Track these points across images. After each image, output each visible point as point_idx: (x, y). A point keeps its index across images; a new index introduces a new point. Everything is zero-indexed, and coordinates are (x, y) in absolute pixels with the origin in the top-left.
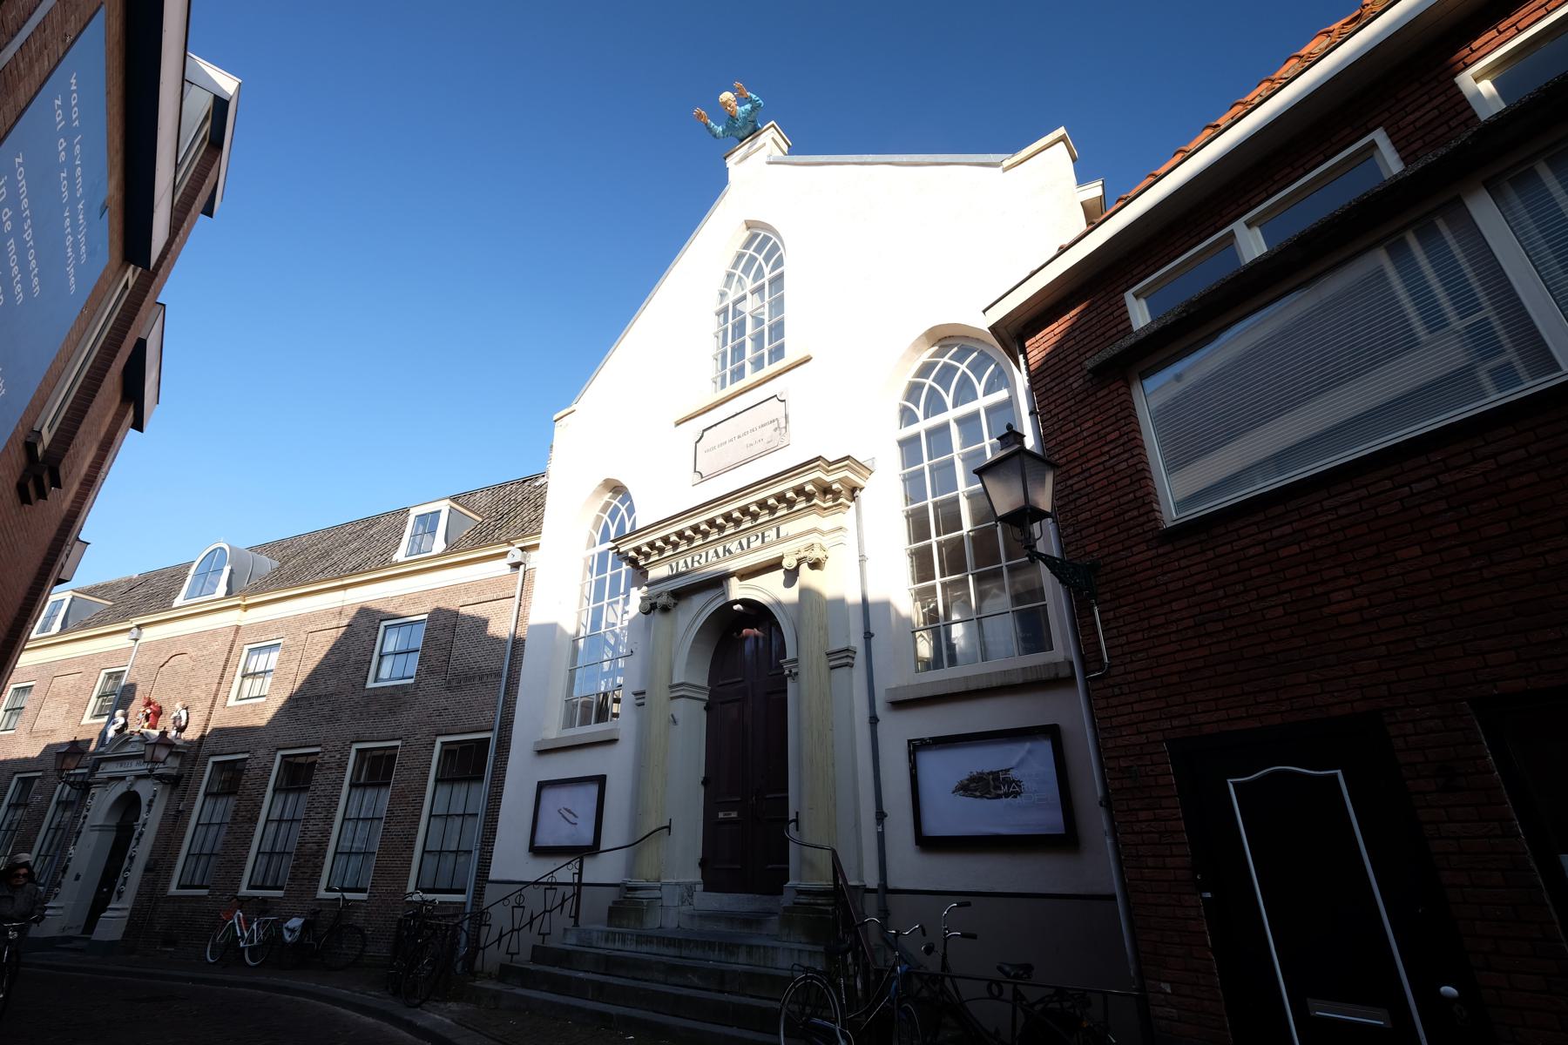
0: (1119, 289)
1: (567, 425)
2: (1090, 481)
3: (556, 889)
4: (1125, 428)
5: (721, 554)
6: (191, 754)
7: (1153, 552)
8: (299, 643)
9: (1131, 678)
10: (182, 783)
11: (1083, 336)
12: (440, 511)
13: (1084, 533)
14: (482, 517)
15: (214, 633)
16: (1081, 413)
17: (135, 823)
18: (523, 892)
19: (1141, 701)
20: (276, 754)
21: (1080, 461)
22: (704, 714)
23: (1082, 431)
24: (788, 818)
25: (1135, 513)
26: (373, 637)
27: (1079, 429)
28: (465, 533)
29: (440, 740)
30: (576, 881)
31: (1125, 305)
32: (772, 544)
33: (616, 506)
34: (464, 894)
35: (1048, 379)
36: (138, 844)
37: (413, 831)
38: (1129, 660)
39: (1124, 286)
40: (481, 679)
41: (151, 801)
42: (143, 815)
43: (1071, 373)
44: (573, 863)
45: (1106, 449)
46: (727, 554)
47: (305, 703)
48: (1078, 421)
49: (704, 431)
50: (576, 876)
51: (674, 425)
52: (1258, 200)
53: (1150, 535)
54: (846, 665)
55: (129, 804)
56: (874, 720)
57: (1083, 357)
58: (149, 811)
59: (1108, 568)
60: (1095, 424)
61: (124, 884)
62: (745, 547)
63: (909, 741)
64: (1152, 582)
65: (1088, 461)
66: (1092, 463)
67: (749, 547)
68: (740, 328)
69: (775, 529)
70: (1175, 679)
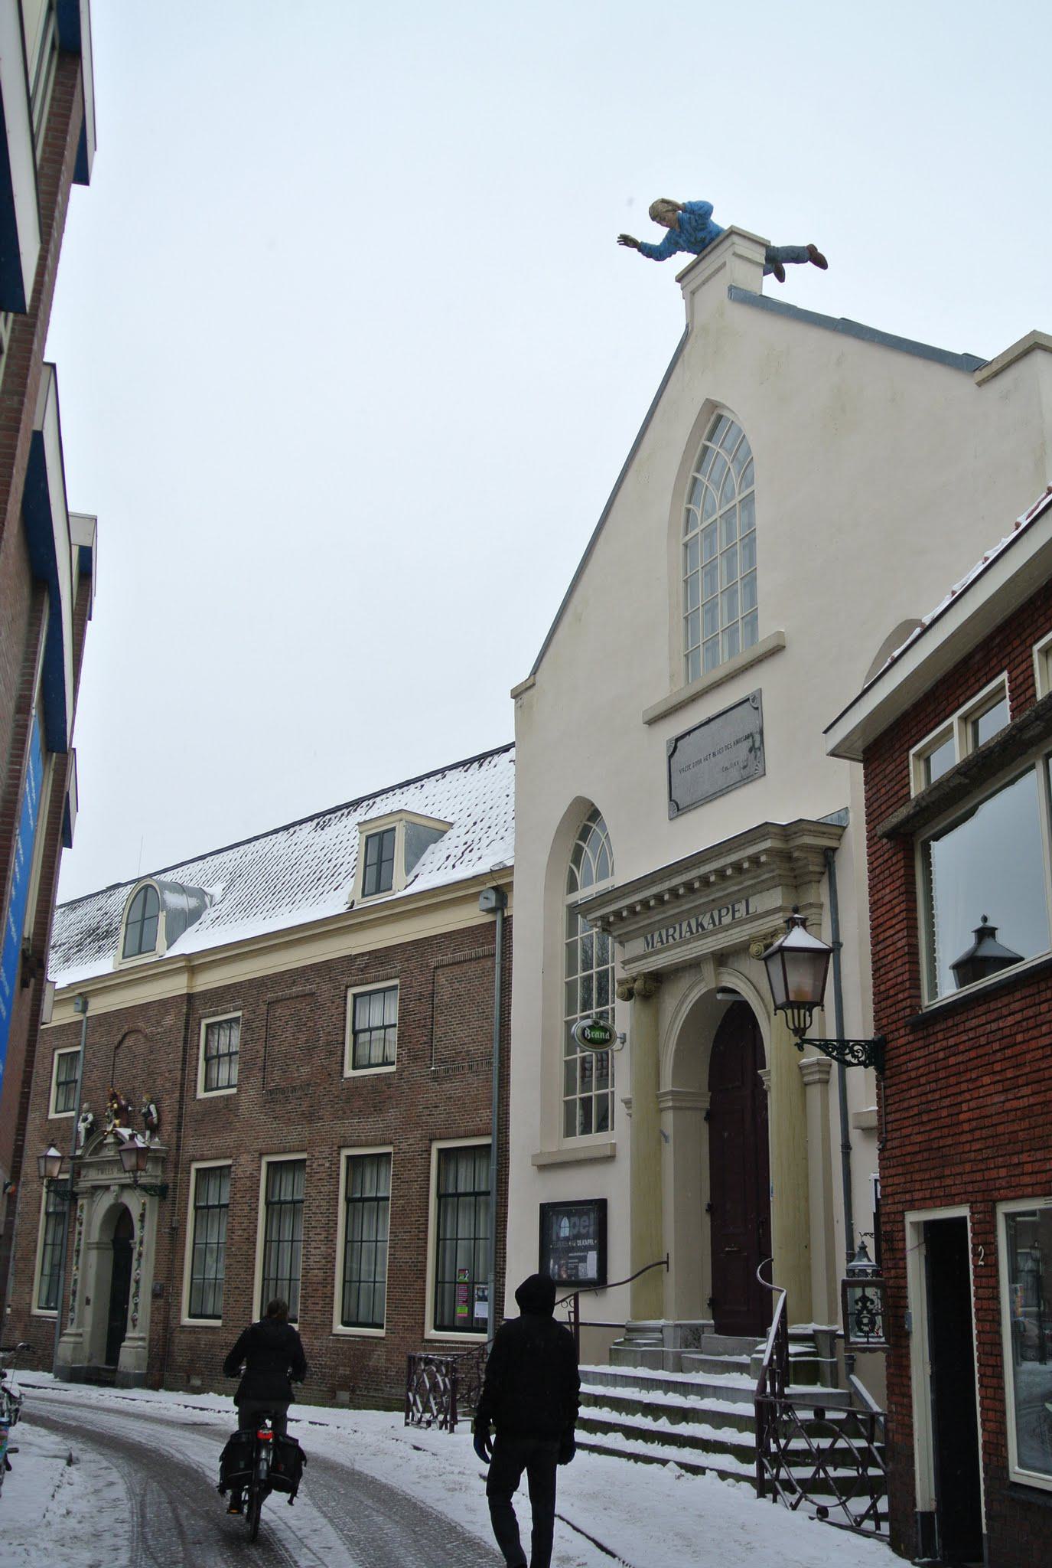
6: (172, 1159)
8: (260, 1017)
10: (170, 1193)
12: (394, 829)
17: (131, 1241)
20: (260, 1160)
26: (341, 1010)
29: (437, 1146)
34: (486, 1333)
36: (139, 1266)
41: (142, 1216)
42: (137, 1233)
44: (568, 1300)
49: (677, 740)
50: (572, 1315)
51: (639, 720)
55: (120, 1222)
56: (846, 1148)
58: (142, 1227)
61: (136, 1310)
62: (694, 931)
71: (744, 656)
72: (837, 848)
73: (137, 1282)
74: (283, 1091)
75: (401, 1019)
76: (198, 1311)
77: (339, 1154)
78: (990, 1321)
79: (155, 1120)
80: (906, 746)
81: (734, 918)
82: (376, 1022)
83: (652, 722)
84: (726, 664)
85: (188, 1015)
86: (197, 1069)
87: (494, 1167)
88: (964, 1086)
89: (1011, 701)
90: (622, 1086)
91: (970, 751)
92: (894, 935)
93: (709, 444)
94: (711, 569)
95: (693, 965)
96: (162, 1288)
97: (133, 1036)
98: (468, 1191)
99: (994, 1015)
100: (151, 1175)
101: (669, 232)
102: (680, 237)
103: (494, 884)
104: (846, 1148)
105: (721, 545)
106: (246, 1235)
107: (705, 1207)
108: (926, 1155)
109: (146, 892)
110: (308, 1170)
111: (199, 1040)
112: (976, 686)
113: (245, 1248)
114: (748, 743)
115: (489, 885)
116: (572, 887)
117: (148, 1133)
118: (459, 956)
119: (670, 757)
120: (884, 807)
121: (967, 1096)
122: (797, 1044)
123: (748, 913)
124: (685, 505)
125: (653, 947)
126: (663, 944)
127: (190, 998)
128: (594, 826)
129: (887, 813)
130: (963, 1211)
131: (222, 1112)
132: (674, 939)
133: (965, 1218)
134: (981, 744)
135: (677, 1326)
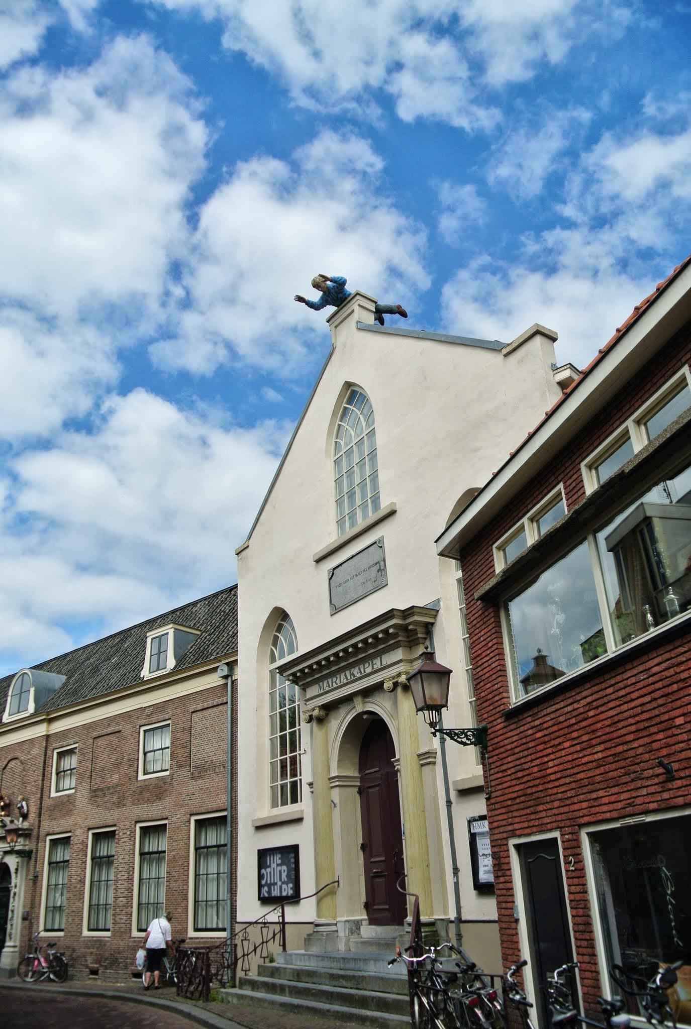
3: (268, 927)
8: (89, 747)
10: (33, 855)
12: (167, 634)
14: (200, 630)
15: (32, 741)
17: (10, 886)
18: (248, 930)
22: (358, 797)
28: (189, 648)
30: (281, 921)
37: (185, 887)
40: (214, 770)
41: (17, 870)
47: (100, 793)
50: (281, 918)
52: (586, 454)
54: (429, 763)
56: (449, 803)
58: (17, 877)
61: (11, 929)
67: (365, 672)
70: (509, 802)
71: (372, 517)
72: (434, 623)
73: (13, 911)
74: (102, 790)
75: (172, 743)
76: (49, 927)
77: (135, 826)
78: (582, 908)
79: (25, 811)
80: (577, 461)
81: (373, 669)
82: (158, 746)
83: (318, 561)
84: (361, 524)
85: (46, 748)
86: (51, 779)
87: (229, 829)
88: (550, 751)
89: (567, 500)
90: (306, 775)
91: (646, 442)
92: (489, 660)
93: (340, 423)
94: (350, 472)
95: (348, 699)
96: (28, 913)
97: (14, 761)
98: (213, 844)
99: (570, 701)
100: (21, 844)
101: (323, 295)
102: (329, 297)
103: (227, 661)
105: (356, 459)
106: (79, 878)
107: (359, 846)
108: (523, 799)
109: (23, 677)
110: (117, 837)
111: (52, 762)
112: (540, 497)
113: (79, 886)
114: (377, 567)
115: (223, 662)
116: (273, 659)
117: (21, 819)
118: (206, 705)
119: (330, 579)
120: (476, 583)
121: (552, 757)
122: (432, 733)
123: (381, 665)
124: (334, 440)
126: (329, 687)
127: (48, 737)
128: (285, 624)
129: (479, 586)
130: (556, 834)
131: (65, 805)
132: (337, 684)
133: (556, 838)
134: (542, 534)
135: (346, 921)
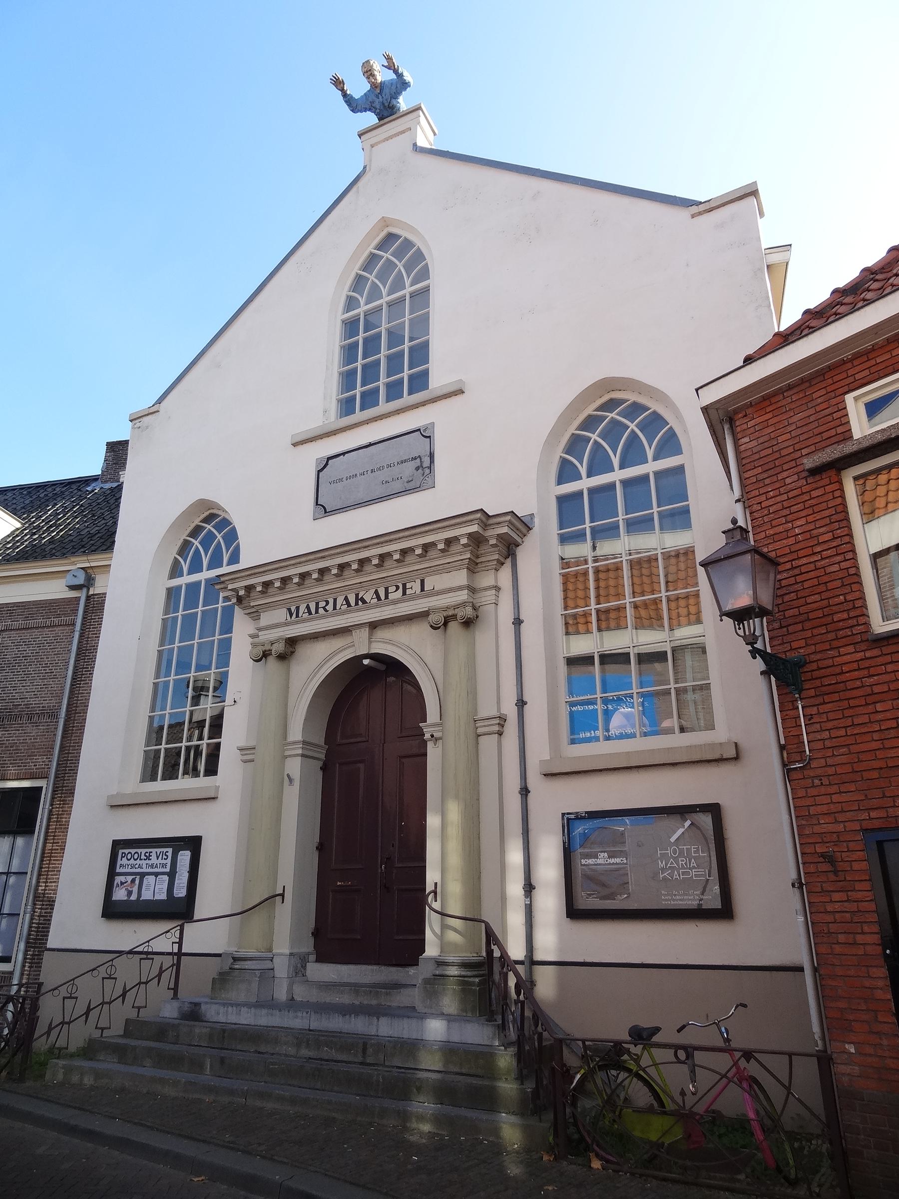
0: (841, 391)
1: (147, 427)
2: (799, 578)
3: (153, 959)
4: (839, 531)
5: (353, 602)
7: (860, 655)
9: (831, 771)
11: (799, 431)
13: (791, 629)
16: (794, 509)
19: (840, 792)
21: (790, 557)
23: (793, 528)
24: (425, 890)
25: (845, 616)
27: (790, 525)
30: (176, 950)
31: (845, 408)
32: (414, 597)
33: (210, 531)
35: (760, 470)
38: (830, 754)
39: (846, 389)
43: (785, 467)
45: (818, 549)
46: (360, 603)
48: (790, 518)
49: (329, 459)
51: (288, 441)
53: (858, 638)
56: (525, 791)
57: (798, 454)
59: (814, 666)
60: (807, 523)
63: (563, 814)
64: (858, 683)
65: (799, 558)
66: (804, 561)
67: (387, 597)
68: (372, 345)
69: (418, 582)
70: (875, 774)
104: (525, 791)
107: (316, 845)
119: (319, 472)
125: (297, 616)
